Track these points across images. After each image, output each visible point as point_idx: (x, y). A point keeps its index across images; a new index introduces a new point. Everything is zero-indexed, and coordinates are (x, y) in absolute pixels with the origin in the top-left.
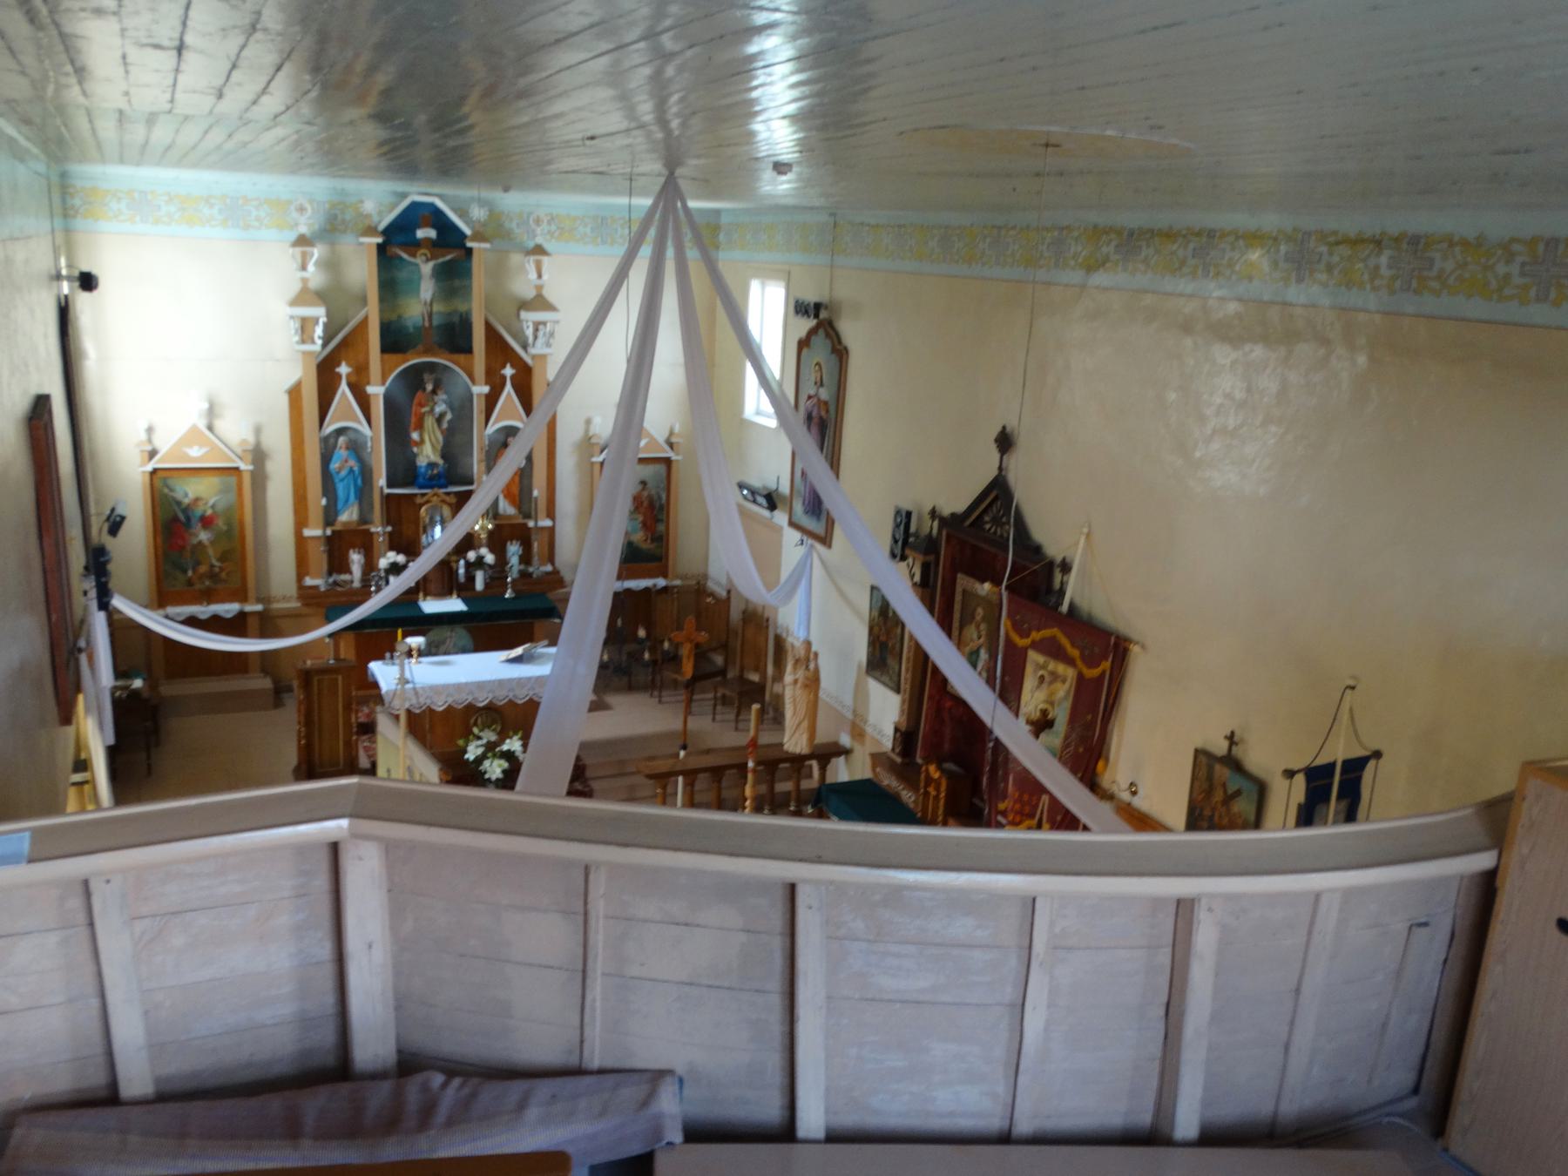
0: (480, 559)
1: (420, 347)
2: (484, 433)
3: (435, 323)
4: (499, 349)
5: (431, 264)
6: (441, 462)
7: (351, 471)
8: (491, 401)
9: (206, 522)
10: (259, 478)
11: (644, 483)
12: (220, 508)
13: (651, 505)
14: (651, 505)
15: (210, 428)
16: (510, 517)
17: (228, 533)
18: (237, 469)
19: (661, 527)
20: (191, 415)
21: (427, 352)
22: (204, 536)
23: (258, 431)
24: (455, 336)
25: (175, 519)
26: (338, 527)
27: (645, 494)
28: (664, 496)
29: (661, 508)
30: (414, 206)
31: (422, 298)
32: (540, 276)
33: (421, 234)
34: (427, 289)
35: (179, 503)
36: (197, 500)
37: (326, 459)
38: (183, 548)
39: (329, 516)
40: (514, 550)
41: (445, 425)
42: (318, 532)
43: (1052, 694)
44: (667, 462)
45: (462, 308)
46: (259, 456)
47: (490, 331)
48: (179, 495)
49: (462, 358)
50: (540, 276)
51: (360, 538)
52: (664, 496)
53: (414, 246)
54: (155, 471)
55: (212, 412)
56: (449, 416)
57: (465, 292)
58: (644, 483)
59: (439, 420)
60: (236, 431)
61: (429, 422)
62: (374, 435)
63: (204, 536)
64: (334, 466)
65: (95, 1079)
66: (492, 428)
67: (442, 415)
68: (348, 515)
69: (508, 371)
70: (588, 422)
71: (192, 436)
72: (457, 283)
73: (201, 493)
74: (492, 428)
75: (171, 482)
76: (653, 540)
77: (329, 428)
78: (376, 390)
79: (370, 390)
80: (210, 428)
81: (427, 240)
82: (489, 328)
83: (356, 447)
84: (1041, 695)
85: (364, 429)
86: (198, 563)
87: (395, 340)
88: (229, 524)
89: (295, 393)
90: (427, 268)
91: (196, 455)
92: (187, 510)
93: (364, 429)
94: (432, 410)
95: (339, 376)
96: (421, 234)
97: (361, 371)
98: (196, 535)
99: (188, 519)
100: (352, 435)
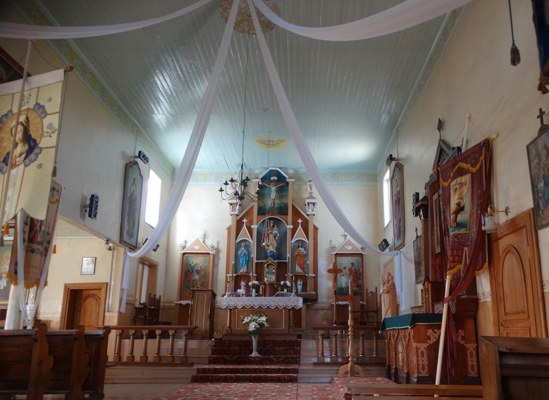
0: (285, 284)
1: (270, 213)
2: (291, 242)
3: (276, 206)
4: (297, 214)
5: (275, 187)
6: (275, 251)
7: (245, 254)
8: (294, 231)
9: (198, 272)
10: (216, 257)
11: (352, 264)
12: (203, 267)
13: (356, 273)
14: (356, 273)
15: (204, 242)
16: (300, 273)
17: (205, 276)
18: (209, 254)
19: (360, 282)
20: (198, 234)
21: (272, 215)
22: (197, 277)
23: (218, 243)
24: (283, 210)
25: (189, 271)
26: (239, 274)
27: (353, 268)
28: (361, 269)
29: (360, 274)
30: (271, 171)
31: (272, 197)
32: (311, 189)
33: (272, 178)
34: (273, 195)
35: (190, 265)
36: (196, 264)
37: (237, 251)
38: (196, 376)
39: (236, 268)
40: (300, 283)
41: (277, 238)
42: (231, 275)
43: (461, 194)
44: (361, 255)
45: (285, 201)
46: (218, 251)
47: (293, 207)
48: (191, 263)
49: (284, 216)
50: (311, 189)
51: (246, 277)
52: (361, 269)
53: (270, 182)
54: (184, 254)
55: (205, 236)
56: (278, 235)
57: (286, 196)
58: (352, 264)
59: (275, 237)
60: (211, 242)
61: (271, 236)
62: (253, 243)
63: (197, 277)
64: (239, 252)
65: (133, 303)
66: (293, 241)
67: (276, 235)
68: (243, 270)
69: (300, 221)
70: (331, 241)
71: (197, 242)
72: (284, 194)
73: (198, 261)
74: (293, 241)
75: (189, 258)
76: (357, 287)
77: (238, 240)
78: (254, 227)
79: (252, 227)
80: (204, 242)
81: (274, 180)
82: (293, 207)
83: (247, 247)
84: (457, 197)
85: (251, 241)
86: (194, 287)
87: (262, 212)
88: (205, 273)
89: (229, 229)
90: (273, 189)
91: (197, 249)
92: (192, 268)
93: (251, 241)
94: (272, 233)
95: (243, 223)
96: (272, 178)
97: (251, 222)
98: (194, 276)
99: (193, 271)
100: (247, 243)
